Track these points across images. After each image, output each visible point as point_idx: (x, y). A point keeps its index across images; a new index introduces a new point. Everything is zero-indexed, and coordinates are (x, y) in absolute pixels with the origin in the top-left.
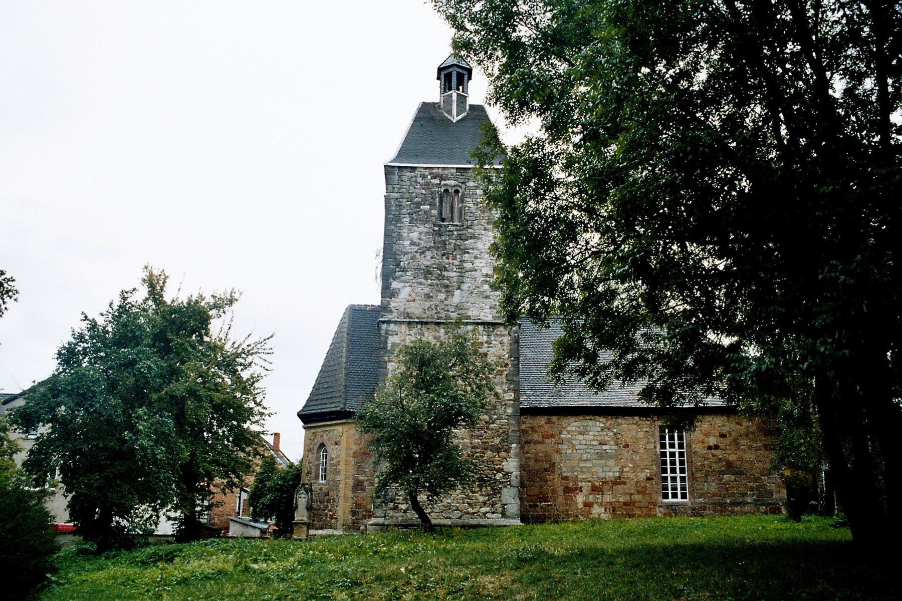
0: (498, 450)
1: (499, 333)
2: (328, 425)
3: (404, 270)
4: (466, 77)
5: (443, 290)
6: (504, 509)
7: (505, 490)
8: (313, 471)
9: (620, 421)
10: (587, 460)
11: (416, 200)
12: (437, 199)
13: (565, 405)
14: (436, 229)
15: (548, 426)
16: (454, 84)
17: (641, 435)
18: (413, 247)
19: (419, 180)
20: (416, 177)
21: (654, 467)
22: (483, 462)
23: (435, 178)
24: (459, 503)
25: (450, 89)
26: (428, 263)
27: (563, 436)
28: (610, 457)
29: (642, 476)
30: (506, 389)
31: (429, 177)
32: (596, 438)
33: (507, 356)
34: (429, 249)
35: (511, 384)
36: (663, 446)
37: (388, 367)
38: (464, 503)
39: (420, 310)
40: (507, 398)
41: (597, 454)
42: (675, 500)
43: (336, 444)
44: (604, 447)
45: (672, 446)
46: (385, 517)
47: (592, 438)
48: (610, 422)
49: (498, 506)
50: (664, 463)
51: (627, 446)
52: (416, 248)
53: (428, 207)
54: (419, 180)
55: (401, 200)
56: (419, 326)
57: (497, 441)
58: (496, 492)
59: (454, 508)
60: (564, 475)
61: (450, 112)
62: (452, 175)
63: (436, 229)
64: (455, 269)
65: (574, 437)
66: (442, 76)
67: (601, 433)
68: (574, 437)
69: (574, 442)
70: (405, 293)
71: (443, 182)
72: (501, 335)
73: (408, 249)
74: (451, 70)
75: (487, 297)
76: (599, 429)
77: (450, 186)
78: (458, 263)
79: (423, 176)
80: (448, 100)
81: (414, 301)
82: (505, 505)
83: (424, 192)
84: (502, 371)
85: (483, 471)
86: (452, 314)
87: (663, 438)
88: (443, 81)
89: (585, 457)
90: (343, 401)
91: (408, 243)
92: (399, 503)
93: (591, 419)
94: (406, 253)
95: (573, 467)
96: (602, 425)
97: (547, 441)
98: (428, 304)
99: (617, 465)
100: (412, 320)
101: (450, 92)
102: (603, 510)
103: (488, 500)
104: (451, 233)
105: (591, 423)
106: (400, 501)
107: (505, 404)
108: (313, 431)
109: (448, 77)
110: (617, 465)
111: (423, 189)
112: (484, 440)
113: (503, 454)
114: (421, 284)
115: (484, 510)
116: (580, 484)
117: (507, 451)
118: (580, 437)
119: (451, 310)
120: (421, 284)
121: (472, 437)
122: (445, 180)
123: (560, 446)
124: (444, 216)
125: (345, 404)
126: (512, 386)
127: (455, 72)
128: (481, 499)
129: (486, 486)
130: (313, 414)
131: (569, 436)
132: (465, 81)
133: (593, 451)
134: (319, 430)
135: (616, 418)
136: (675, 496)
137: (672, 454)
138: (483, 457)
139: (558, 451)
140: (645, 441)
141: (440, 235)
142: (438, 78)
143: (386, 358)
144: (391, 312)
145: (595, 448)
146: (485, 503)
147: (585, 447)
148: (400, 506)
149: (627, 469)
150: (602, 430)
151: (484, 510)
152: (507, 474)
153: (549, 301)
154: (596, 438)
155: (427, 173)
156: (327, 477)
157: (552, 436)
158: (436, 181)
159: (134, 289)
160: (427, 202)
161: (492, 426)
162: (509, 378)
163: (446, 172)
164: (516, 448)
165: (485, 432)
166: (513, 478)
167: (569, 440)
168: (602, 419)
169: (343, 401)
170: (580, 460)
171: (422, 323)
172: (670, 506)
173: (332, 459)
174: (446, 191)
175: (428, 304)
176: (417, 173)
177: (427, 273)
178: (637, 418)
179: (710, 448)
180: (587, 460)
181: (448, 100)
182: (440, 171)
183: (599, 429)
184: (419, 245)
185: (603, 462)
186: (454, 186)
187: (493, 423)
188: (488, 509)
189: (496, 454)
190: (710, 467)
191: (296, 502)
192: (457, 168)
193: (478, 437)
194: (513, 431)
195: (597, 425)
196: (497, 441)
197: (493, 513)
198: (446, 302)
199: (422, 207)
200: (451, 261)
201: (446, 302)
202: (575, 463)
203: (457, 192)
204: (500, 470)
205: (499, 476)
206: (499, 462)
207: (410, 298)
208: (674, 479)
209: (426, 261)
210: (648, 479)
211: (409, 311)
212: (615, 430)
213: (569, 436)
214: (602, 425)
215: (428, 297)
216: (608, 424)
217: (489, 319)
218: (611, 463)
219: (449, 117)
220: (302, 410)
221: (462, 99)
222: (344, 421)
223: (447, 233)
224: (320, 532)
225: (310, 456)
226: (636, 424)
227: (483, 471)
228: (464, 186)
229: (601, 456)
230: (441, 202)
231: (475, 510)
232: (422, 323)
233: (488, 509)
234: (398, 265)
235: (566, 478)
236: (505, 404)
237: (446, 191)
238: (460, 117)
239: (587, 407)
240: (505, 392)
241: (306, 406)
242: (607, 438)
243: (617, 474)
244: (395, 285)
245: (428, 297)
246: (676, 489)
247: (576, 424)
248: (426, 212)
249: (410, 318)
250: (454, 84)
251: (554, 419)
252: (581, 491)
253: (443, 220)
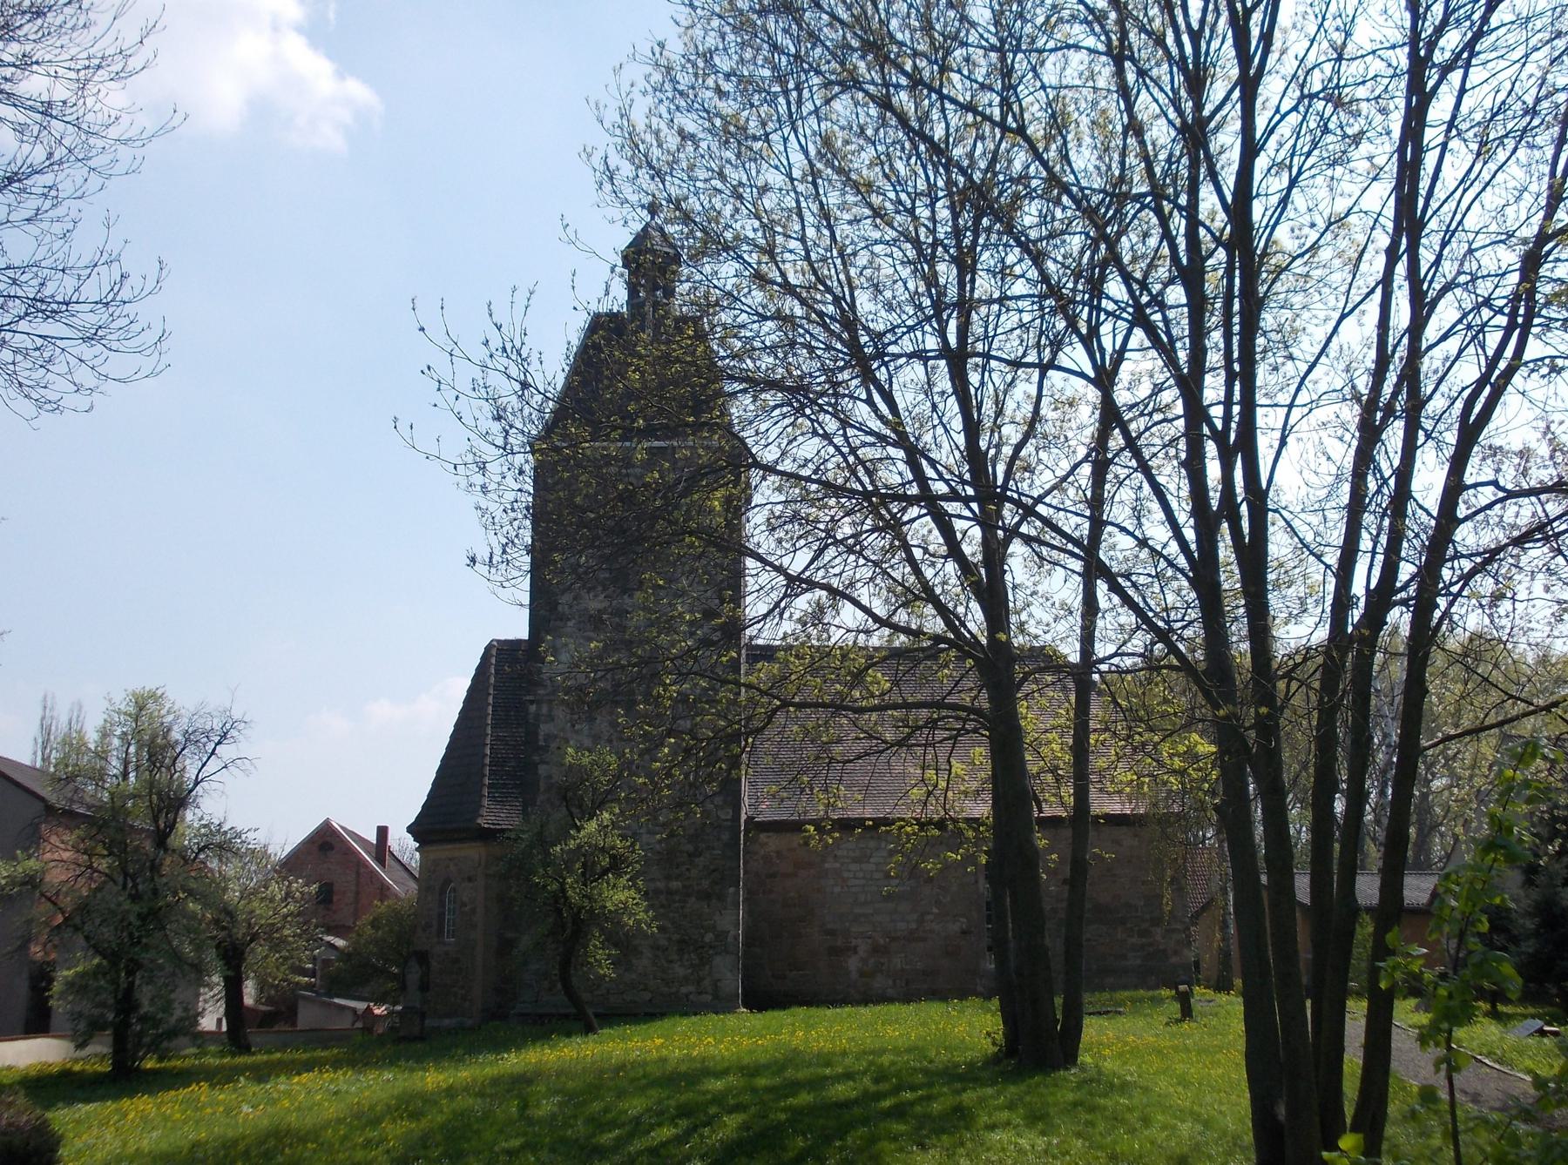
0: (706, 896)
21: (265, 1122)
27: (827, 865)
29: (955, 927)
49: (707, 982)
57: (706, 884)
69: (846, 875)
89: (862, 898)
102: (890, 982)
116: (854, 942)
118: (854, 867)
121: (668, 878)
131: (838, 865)
143: (536, 758)
147: (863, 882)
149: (931, 917)
153: (644, 650)
210: (964, 932)
213: (838, 865)
223: (802, 542)
224: (447, 1022)
235: (832, 933)
243: (914, 926)
252: (856, 953)
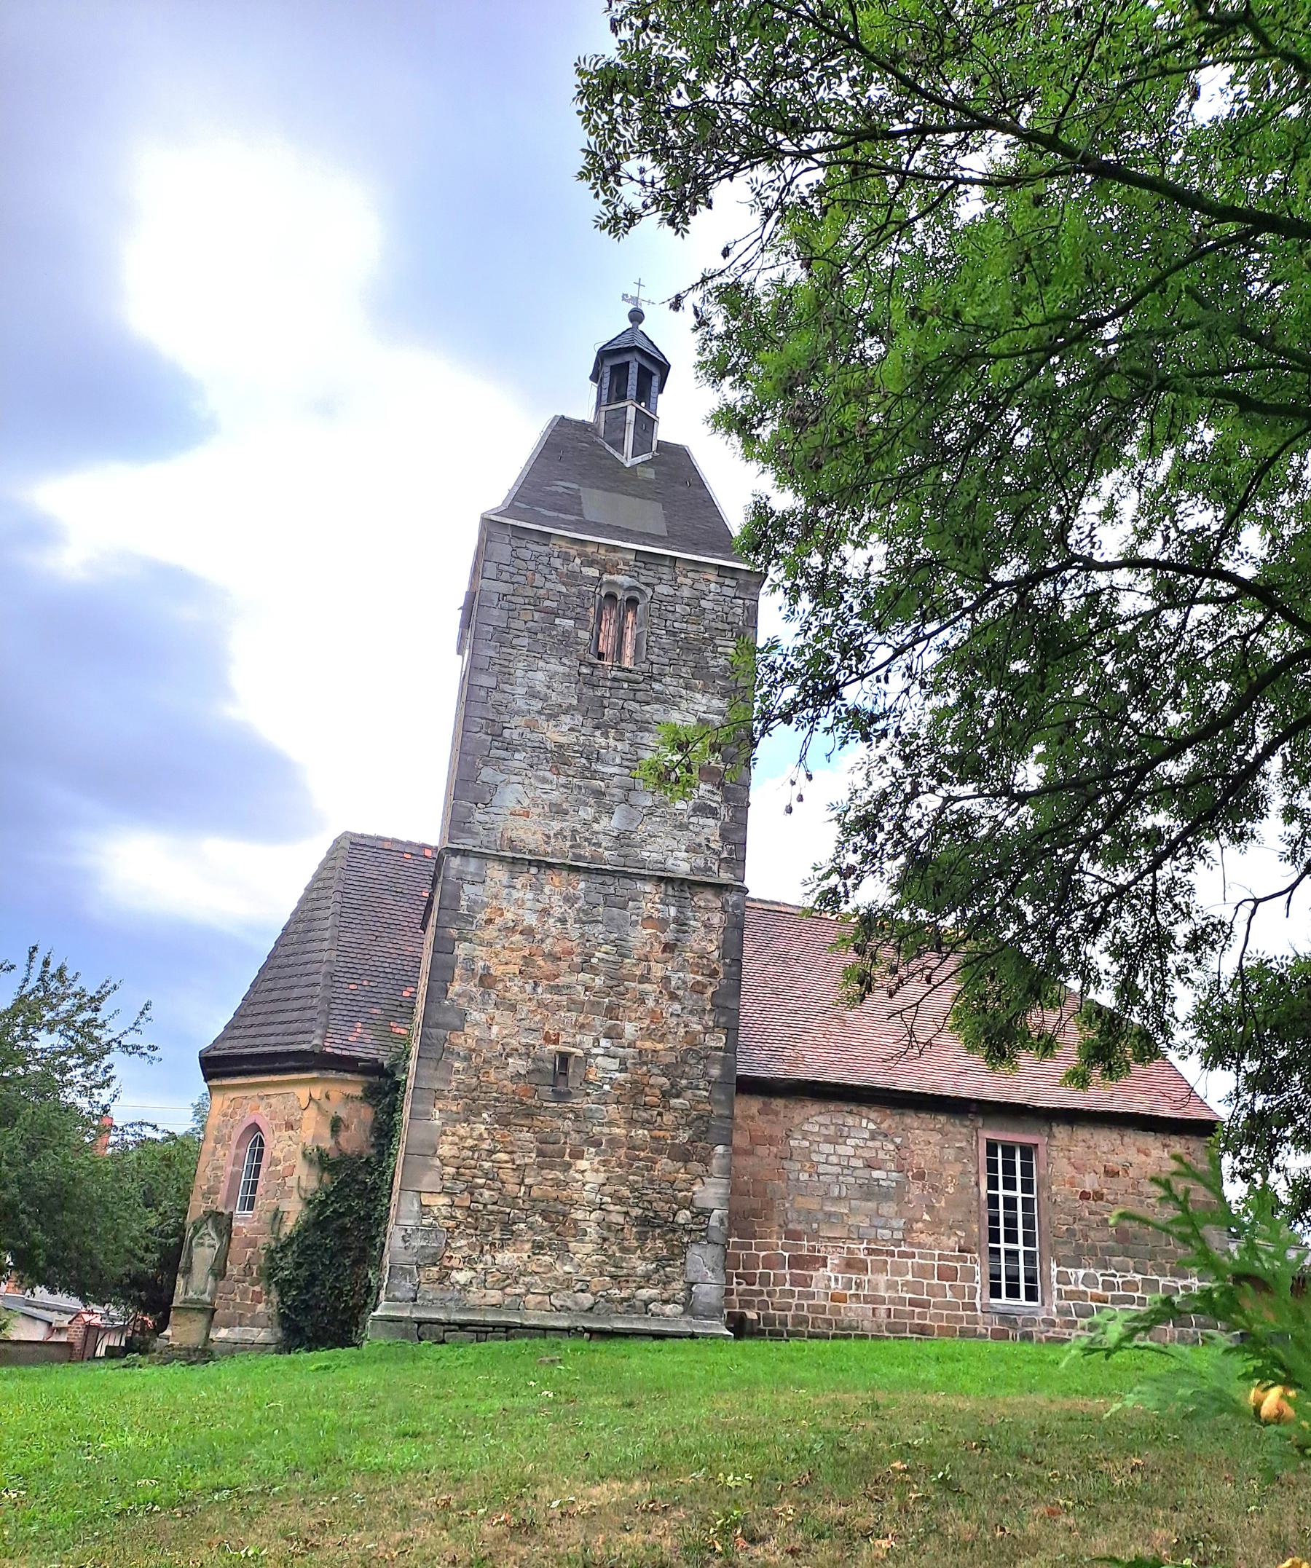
0: (683, 1155)
1: (702, 904)
3: (509, 747)
4: (655, 381)
5: (592, 801)
6: (691, 1292)
8: (224, 1188)
9: (908, 1121)
10: (839, 1198)
11: (547, 603)
12: (592, 610)
13: (802, 1076)
14: (585, 670)
15: (765, 1118)
16: (632, 388)
17: (950, 1154)
18: (533, 702)
19: (557, 563)
20: (549, 555)
22: (651, 1181)
23: (591, 564)
24: (591, 1274)
25: (623, 397)
26: (562, 740)
28: (886, 1195)
30: (711, 1024)
31: (578, 561)
32: (859, 1152)
33: (716, 953)
36: (993, 1184)
38: (602, 1275)
39: (539, 836)
40: (713, 1044)
41: (860, 1186)
42: (1013, 1302)
43: (289, 1126)
44: (876, 1174)
45: (1010, 1184)
46: (415, 1300)
47: (851, 1152)
48: (889, 1121)
50: (994, 1220)
51: (920, 1176)
52: (538, 705)
53: (571, 622)
54: (557, 563)
55: (513, 599)
56: (534, 870)
58: (677, 1253)
59: (578, 1286)
60: (791, 1226)
61: (619, 445)
62: (626, 564)
63: (585, 670)
64: (618, 761)
65: (815, 1147)
66: (606, 371)
67: (870, 1144)
68: (815, 1147)
69: (815, 1157)
70: (510, 796)
71: (606, 577)
72: (708, 910)
73: (521, 704)
74: (627, 358)
75: (683, 827)
76: (867, 1136)
77: (621, 586)
78: (627, 748)
79: (567, 558)
80: (615, 423)
81: (527, 814)
82: (693, 1284)
83: (564, 589)
84: (705, 987)
85: (650, 1202)
86: (607, 853)
87: (992, 1166)
88: (606, 385)
89: (835, 1191)
90: (319, 1032)
91: (521, 690)
92: (452, 1268)
93: (851, 1112)
94: (517, 713)
95: (809, 1212)
96: (872, 1126)
97: (762, 1150)
98: (556, 826)
99: (899, 1214)
100: (518, 856)
101: (622, 405)
103: (656, 1271)
104: (616, 684)
105: (850, 1121)
106: (454, 1263)
107: (707, 1058)
108: (232, 1095)
109: (620, 372)
110: (899, 1214)
111: (564, 584)
112: (657, 1133)
113: (696, 1167)
114: (544, 780)
115: (645, 1293)
117: (705, 1161)
118: (827, 1148)
119: (604, 844)
120: (544, 780)
121: (631, 1122)
122: (611, 573)
123: (786, 1164)
124: (602, 648)
125: (324, 1038)
126: (722, 1020)
127: (636, 365)
128: (642, 1268)
129: (654, 1239)
132: (655, 389)
133: (852, 1180)
134: (254, 1093)
135: (902, 1114)
136: (1013, 1292)
137: (1010, 1203)
138: (650, 1169)
139: (783, 1175)
140: (959, 1167)
141: (594, 686)
142: (595, 377)
144: (474, 834)
145: (858, 1173)
146: (647, 1277)
148: (454, 1273)
150: (873, 1138)
151: (645, 1293)
152: (705, 1213)
154: (859, 1152)
155: (573, 552)
156: (258, 1203)
157: (771, 1141)
158: (593, 572)
160: (568, 613)
161: (674, 1102)
162: (719, 1001)
163: (615, 556)
164: (723, 1156)
165: (660, 1114)
166: (714, 1222)
167: (807, 1153)
168: (873, 1115)
169: (319, 1032)
170: (826, 1196)
171: (540, 864)
172: (1005, 1316)
173: (274, 1162)
174: (611, 597)
175: (556, 826)
176: (556, 547)
177: (559, 757)
178: (942, 1119)
179: (1085, 1196)
180: (839, 1198)
181: (615, 423)
182: (602, 551)
183: (867, 1136)
184: (545, 698)
185: (871, 1205)
186: (630, 588)
187: (678, 1096)
188: (653, 1292)
189: (680, 1164)
190: (1086, 1238)
191: (190, 1258)
192: (637, 551)
193: (645, 1123)
194: (720, 1116)
195: (864, 1123)
196: (684, 1136)
197: (666, 1302)
198: (596, 827)
199: (557, 621)
200: (612, 742)
201: (596, 827)
202: (813, 1204)
203: (633, 602)
206: (684, 1185)
207: (518, 807)
208: (1012, 1255)
209: (555, 734)
212: (898, 1140)
214: (872, 1126)
215: (558, 811)
216: (885, 1126)
217: (682, 865)
218: (888, 1208)
219: (617, 455)
220: (214, 1046)
221: (647, 423)
222: (315, 1075)
223: (608, 684)
225: (220, 1153)
226: (940, 1131)
227: (650, 1202)
228: (649, 591)
229: (870, 1191)
230: (599, 619)
231: (625, 1294)
232: (540, 864)
233: (653, 1292)
234: (497, 736)
236: (707, 1058)
237: (611, 597)
238: (639, 459)
239: (844, 1086)
240: (707, 1030)
241: (222, 1038)
242: (881, 1155)
245: (558, 811)
246: (1017, 1279)
247: (821, 1119)
248: (566, 634)
249: (513, 849)
250: (632, 388)
251: (778, 1104)
253: (601, 656)
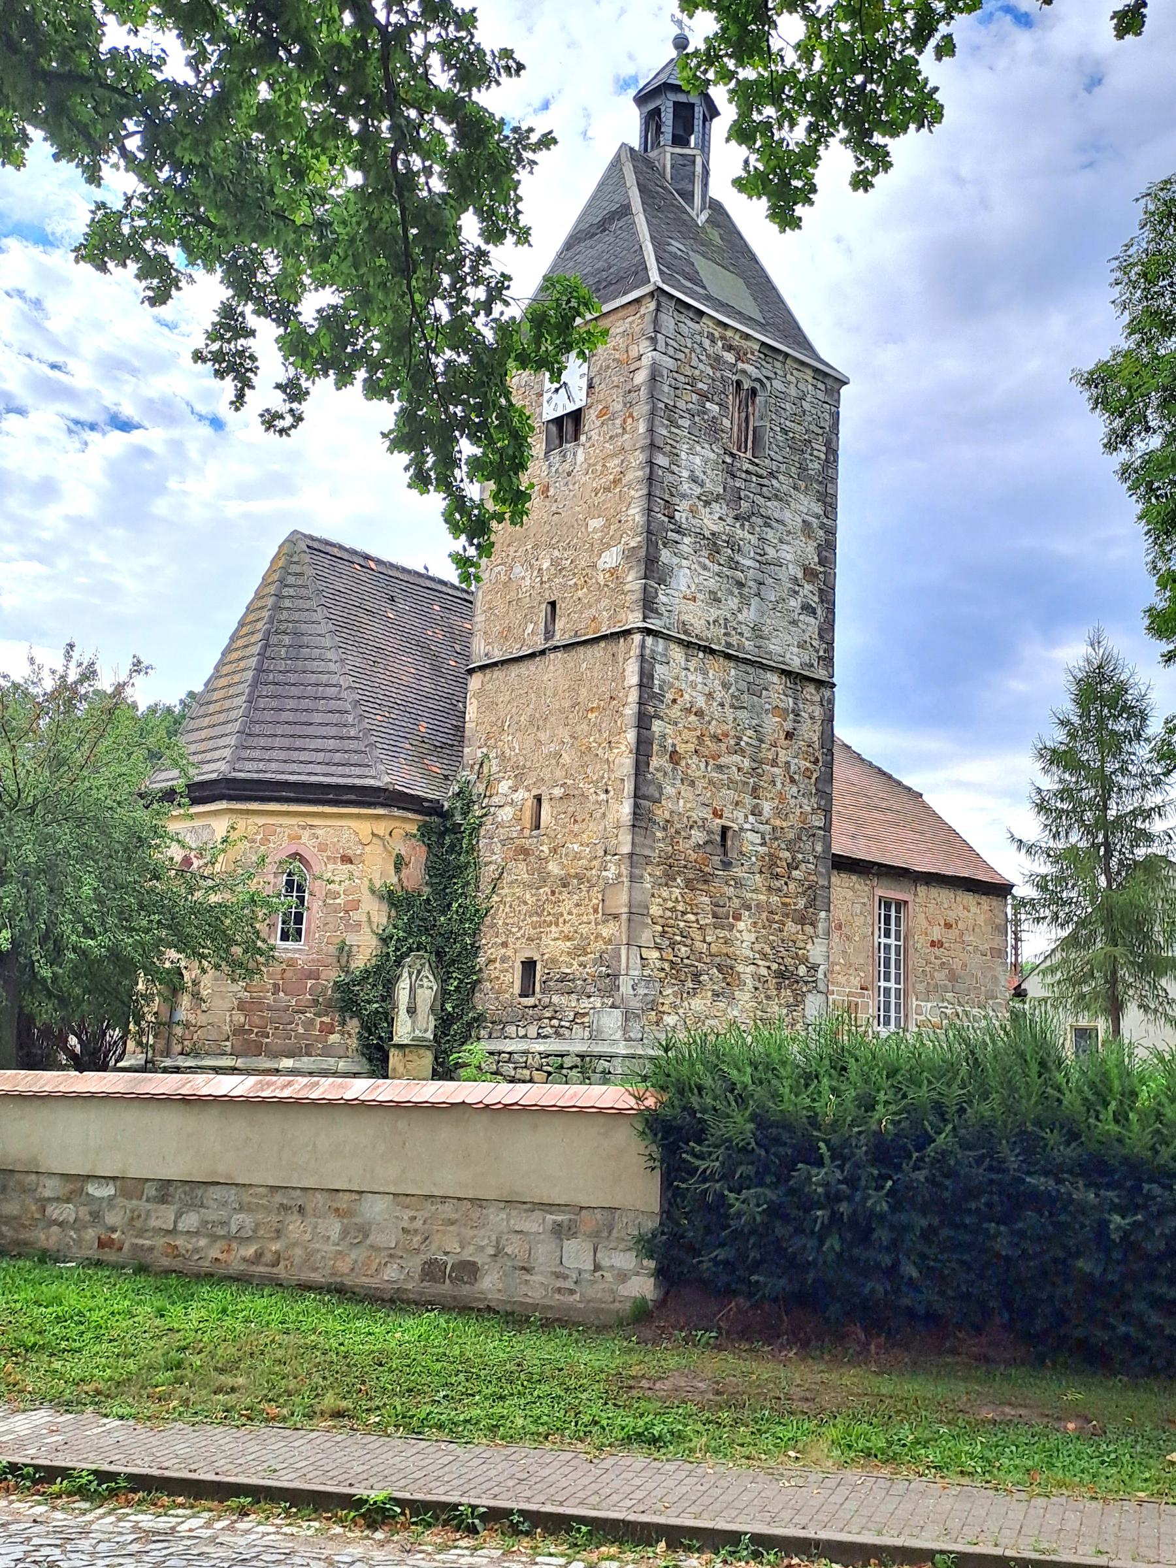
2: (350, 816)
7: (809, 996)
34: (717, 499)
35: (821, 798)
37: (654, 728)
39: (703, 622)
52: (698, 491)
64: (752, 554)
71: (740, 365)
75: (794, 623)
81: (694, 599)
86: (747, 643)
107: (814, 835)
113: (809, 929)
130: (244, 781)
158: (730, 357)
159: (839, 240)
161: (795, 873)
165: (786, 884)
175: (714, 613)
179: (933, 944)
192: (763, 343)
204: (804, 960)
205: (802, 970)
211: (684, 617)
236: (814, 835)
244: (665, 555)
249: (686, 633)
